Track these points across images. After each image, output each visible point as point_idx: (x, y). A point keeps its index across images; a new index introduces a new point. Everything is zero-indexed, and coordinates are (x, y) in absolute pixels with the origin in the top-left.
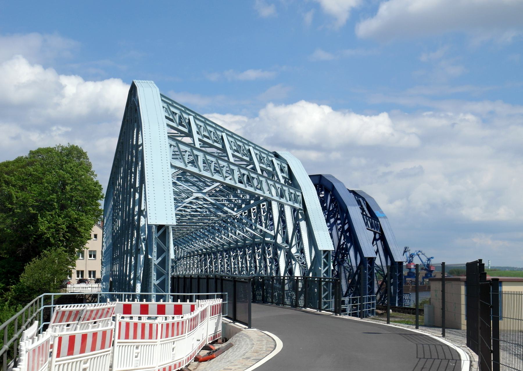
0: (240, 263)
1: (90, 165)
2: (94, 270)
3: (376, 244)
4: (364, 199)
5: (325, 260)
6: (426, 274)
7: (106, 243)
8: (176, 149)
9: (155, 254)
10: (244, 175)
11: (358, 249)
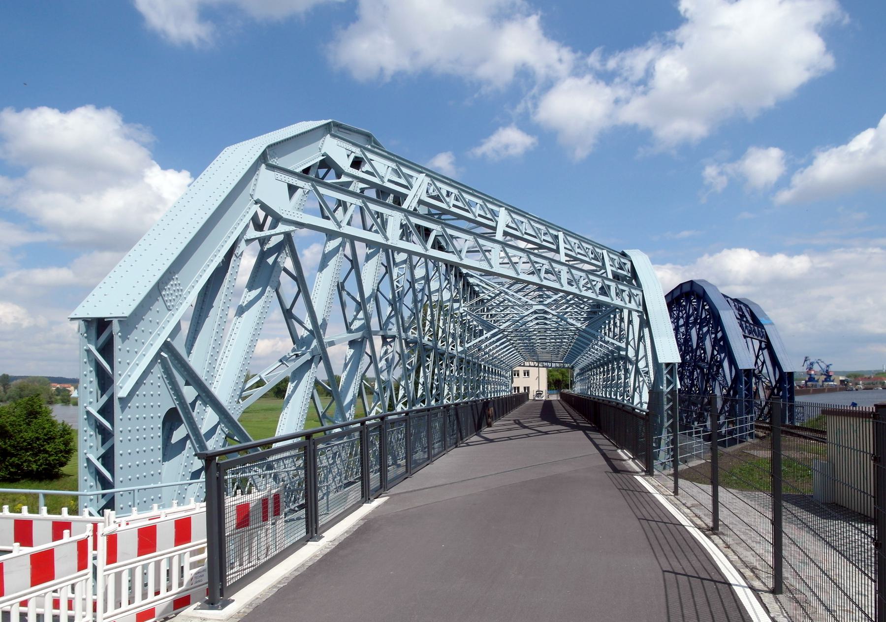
3: (763, 353)
4: (746, 306)
5: (669, 377)
6: (825, 379)
11: (733, 362)
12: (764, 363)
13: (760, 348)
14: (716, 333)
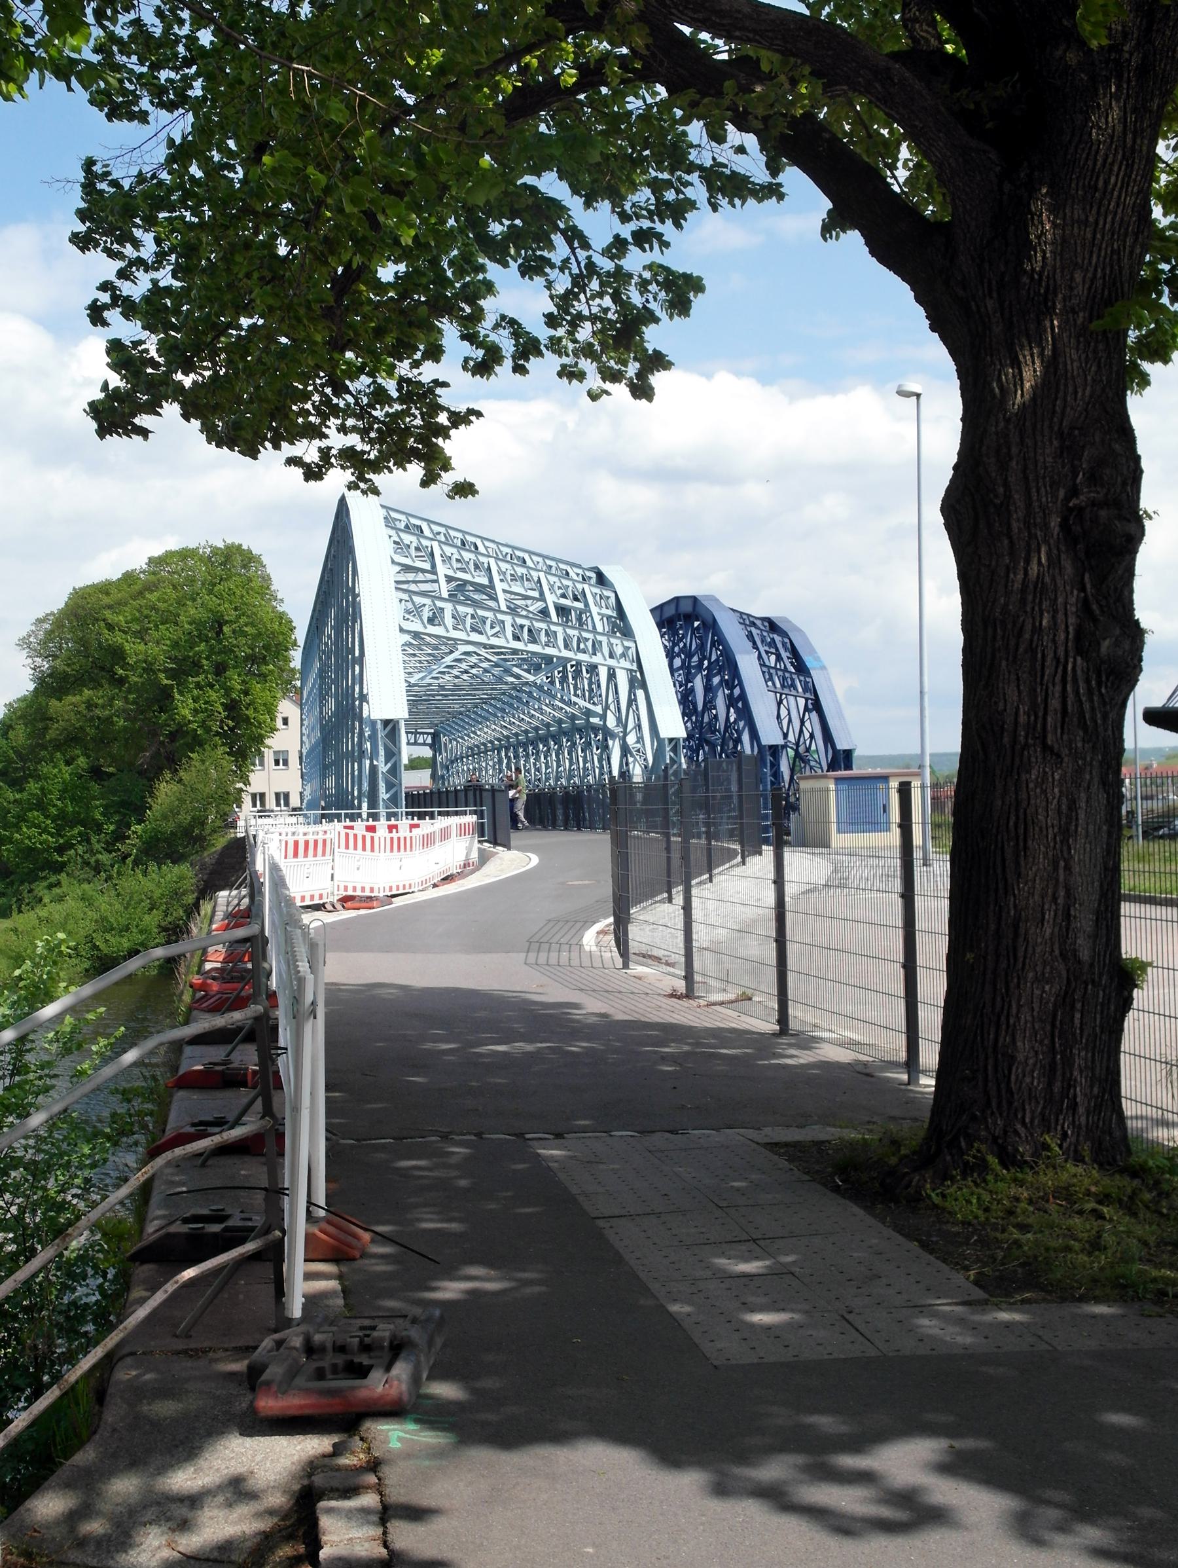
0: (581, 760)
1: (267, 579)
2: (285, 790)
4: (784, 634)
7: (308, 736)
8: (410, 605)
9: (382, 758)
10: (522, 627)
11: (754, 735)
12: (812, 736)
13: (806, 709)
14: (732, 688)
